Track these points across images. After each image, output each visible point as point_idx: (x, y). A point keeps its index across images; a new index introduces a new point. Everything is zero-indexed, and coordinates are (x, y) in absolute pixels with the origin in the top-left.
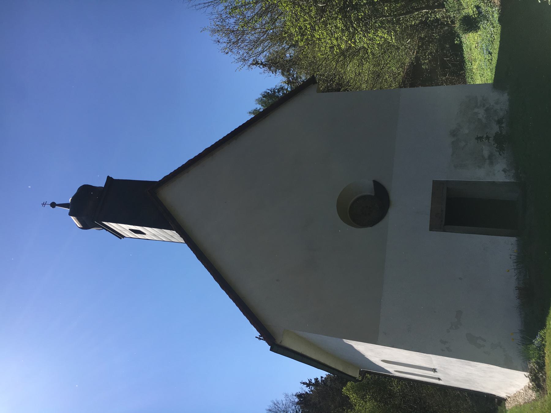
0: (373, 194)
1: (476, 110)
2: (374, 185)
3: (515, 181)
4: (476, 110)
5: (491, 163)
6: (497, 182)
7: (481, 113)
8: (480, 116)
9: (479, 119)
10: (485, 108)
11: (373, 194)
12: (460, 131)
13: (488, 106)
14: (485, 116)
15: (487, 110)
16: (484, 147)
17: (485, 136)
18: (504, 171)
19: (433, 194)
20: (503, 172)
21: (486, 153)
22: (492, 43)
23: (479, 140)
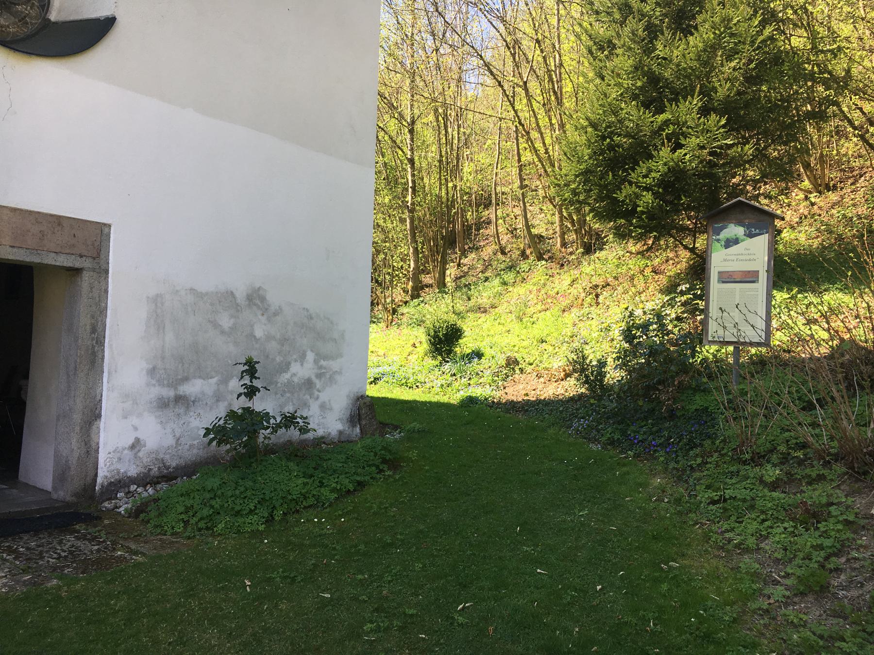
0: (53, 16)
1: (310, 356)
2: (96, 21)
3: (99, 480)
4: (310, 356)
5: (163, 404)
6: (98, 428)
7: (301, 371)
8: (295, 368)
9: (290, 363)
10: (313, 378)
11: (53, 16)
12: (263, 315)
13: (318, 386)
14: (296, 380)
15: (308, 384)
16: (215, 380)
17: (257, 383)
18: (136, 445)
19: (58, 220)
20: (131, 441)
21: (194, 388)
22: (403, 385)
23: (246, 367)
